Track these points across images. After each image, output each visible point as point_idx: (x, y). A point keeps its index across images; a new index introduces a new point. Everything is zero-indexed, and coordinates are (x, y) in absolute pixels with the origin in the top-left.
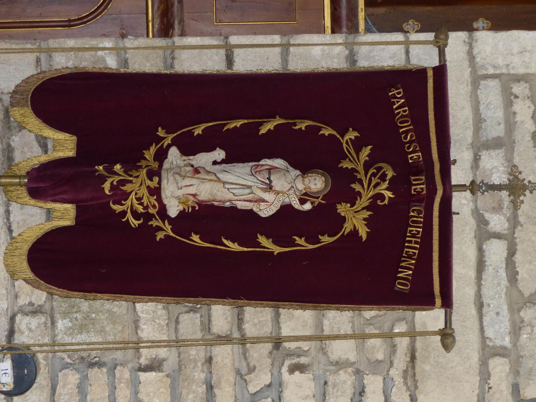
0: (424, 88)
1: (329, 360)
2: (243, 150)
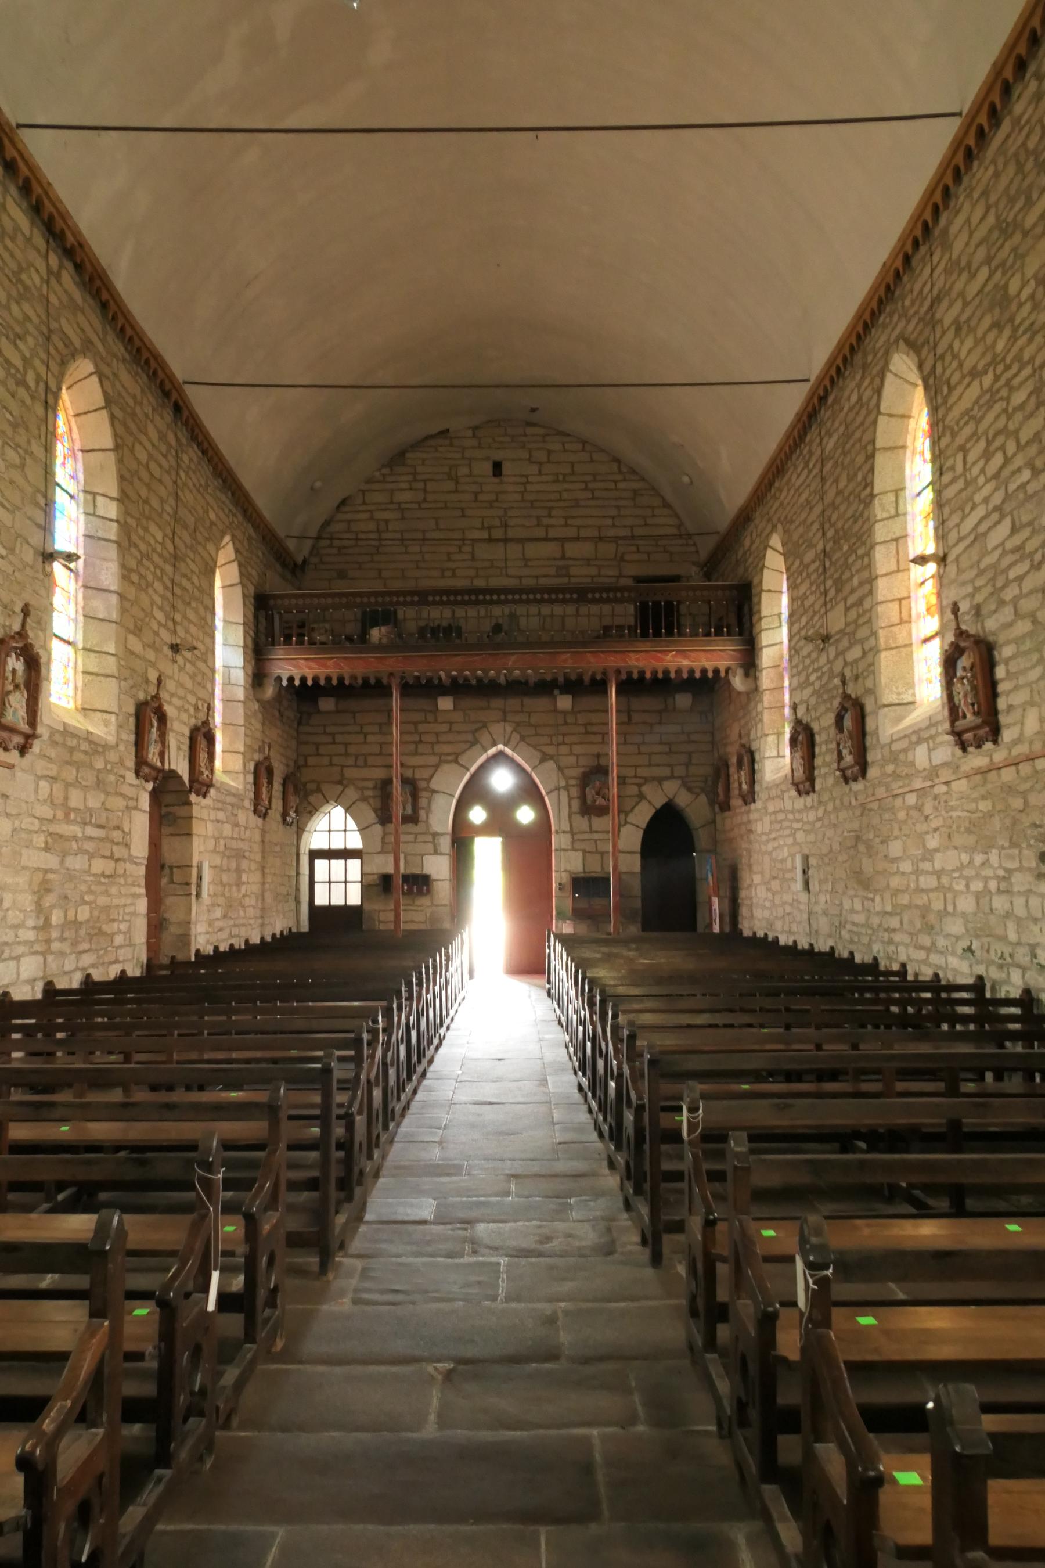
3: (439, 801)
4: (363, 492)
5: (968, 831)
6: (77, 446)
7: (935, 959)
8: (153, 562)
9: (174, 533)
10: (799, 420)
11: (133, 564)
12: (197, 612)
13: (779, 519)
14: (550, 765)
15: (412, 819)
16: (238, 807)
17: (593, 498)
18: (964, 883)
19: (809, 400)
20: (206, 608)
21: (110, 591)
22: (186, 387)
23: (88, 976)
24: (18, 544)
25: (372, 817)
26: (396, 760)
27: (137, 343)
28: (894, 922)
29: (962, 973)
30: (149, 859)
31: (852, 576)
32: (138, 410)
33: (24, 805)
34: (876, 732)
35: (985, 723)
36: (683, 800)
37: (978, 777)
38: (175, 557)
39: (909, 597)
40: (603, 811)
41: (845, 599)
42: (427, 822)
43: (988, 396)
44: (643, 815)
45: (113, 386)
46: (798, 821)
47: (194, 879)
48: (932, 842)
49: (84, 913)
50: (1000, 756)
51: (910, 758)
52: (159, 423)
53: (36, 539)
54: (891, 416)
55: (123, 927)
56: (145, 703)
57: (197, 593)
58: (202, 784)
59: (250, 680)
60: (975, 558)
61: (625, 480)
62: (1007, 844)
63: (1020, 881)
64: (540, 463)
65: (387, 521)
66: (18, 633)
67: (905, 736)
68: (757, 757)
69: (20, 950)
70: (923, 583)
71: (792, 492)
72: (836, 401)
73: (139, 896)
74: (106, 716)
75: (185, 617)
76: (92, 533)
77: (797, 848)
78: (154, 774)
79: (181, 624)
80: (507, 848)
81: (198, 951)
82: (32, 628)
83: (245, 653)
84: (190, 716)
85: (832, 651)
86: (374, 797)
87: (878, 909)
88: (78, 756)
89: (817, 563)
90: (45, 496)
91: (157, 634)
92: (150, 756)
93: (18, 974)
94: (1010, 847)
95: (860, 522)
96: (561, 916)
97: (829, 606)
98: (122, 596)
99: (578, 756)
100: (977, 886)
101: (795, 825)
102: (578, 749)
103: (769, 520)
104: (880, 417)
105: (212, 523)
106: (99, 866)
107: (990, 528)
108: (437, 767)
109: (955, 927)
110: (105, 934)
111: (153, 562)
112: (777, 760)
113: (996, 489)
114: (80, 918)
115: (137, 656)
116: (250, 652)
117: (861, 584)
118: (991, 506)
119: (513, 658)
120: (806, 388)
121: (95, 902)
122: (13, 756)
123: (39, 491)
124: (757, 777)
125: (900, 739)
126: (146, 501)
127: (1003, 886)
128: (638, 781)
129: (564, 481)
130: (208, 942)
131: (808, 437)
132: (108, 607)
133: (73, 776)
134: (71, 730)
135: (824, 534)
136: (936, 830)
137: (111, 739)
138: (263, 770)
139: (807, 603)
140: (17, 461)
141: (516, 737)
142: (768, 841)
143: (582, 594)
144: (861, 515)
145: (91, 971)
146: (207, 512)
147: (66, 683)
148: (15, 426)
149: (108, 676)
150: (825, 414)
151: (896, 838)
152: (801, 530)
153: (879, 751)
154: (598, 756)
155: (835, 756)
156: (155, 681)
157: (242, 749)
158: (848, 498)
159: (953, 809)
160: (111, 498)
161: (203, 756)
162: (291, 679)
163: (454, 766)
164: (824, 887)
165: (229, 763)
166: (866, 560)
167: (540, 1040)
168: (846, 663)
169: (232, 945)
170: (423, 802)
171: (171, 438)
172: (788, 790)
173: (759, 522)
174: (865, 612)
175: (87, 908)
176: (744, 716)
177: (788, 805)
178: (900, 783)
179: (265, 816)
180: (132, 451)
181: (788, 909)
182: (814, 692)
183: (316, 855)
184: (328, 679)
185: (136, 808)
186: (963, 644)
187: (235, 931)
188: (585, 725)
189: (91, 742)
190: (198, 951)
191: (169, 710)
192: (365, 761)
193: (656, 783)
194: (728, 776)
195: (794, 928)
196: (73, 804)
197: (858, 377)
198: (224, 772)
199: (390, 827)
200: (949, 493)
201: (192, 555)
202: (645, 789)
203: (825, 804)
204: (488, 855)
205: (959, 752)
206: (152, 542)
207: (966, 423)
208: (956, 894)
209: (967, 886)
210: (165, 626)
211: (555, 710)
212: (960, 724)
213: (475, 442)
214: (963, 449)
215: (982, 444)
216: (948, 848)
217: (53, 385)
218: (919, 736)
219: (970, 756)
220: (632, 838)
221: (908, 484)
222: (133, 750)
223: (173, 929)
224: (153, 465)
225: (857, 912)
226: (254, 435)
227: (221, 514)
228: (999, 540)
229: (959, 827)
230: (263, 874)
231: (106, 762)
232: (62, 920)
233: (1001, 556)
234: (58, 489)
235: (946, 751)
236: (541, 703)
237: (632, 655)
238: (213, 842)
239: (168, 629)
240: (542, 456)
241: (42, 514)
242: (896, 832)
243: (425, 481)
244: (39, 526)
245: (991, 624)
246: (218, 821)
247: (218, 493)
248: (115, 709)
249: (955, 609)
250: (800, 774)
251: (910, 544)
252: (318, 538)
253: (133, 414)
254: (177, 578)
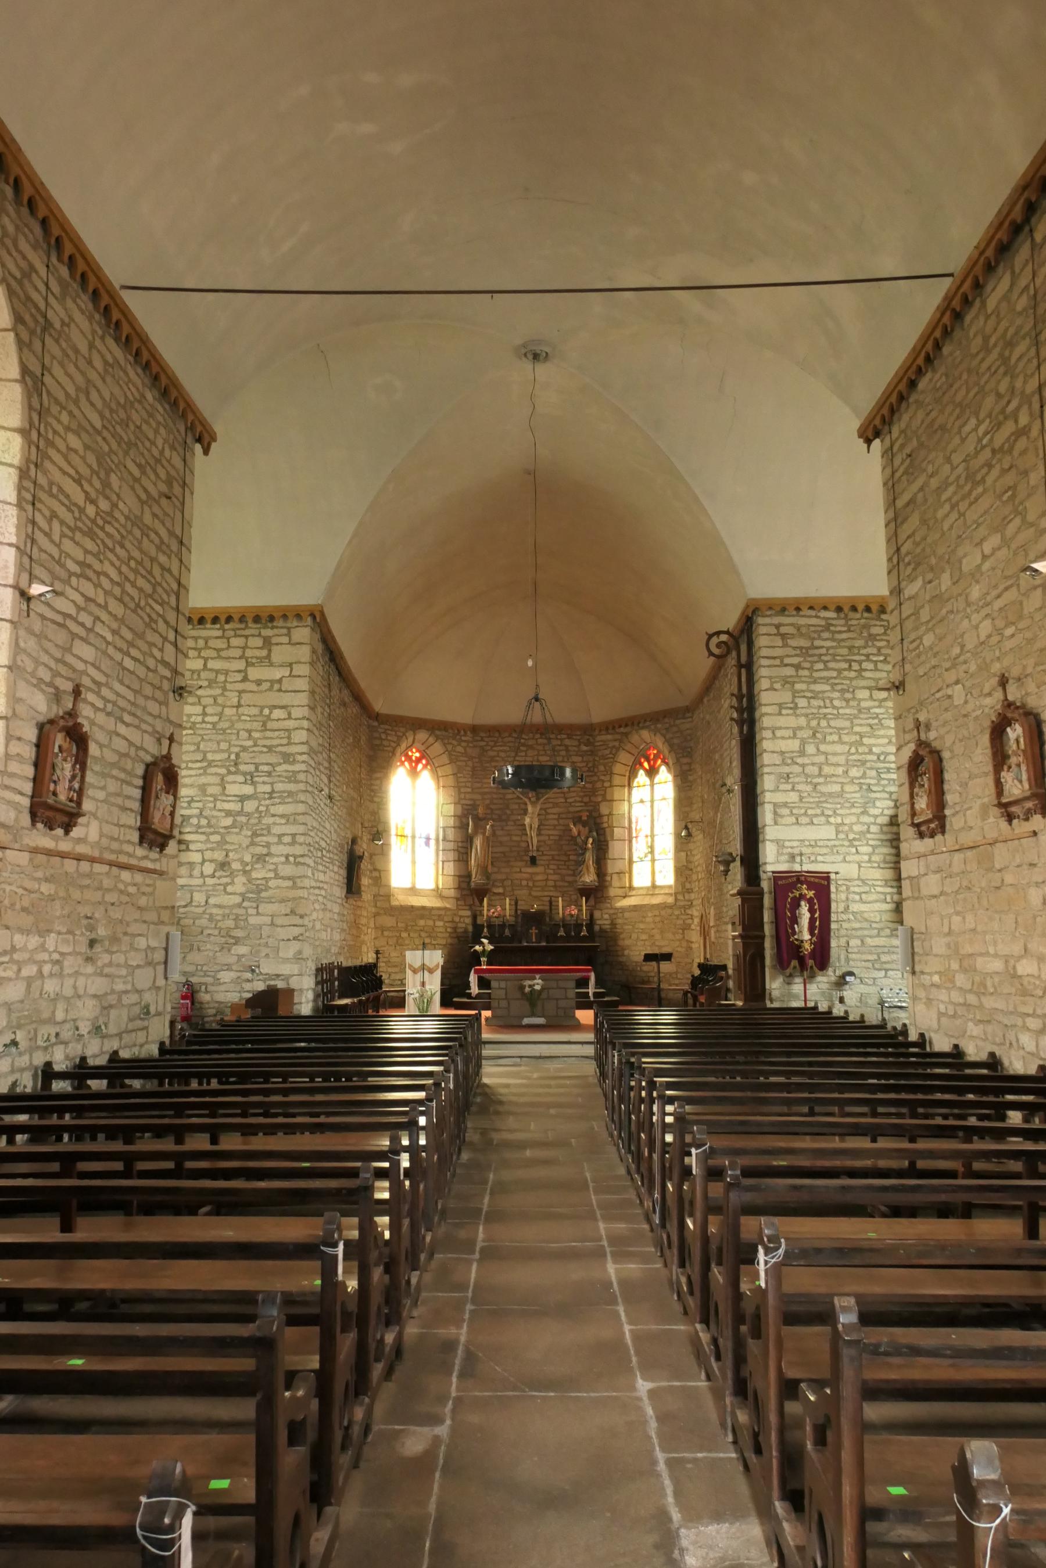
0: (778, 878)
1: (1006, 699)
2: (795, 920)
18: (15, 968)
27: (155, 369)
50: (65, 846)
63: (70, 964)
120: (947, 283)
186: (1009, 715)
229: (13, 905)
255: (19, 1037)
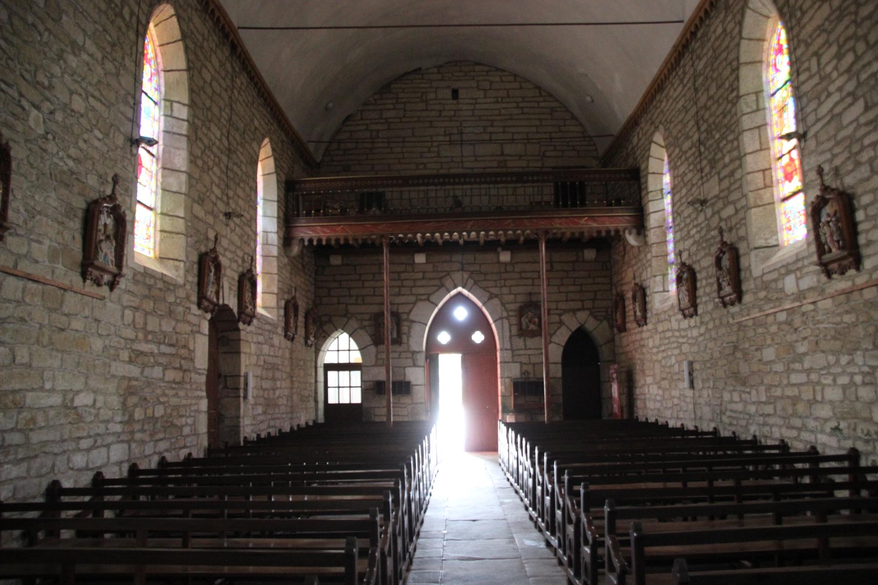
3: (416, 328)
4: (362, 111)
5: (834, 338)
6: (161, 67)
7: (806, 436)
8: (213, 153)
9: (228, 133)
10: (675, 51)
11: (199, 153)
12: (244, 190)
13: (660, 122)
14: (496, 301)
15: (398, 341)
16: (273, 333)
17: (522, 113)
18: (831, 378)
19: (683, 35)
20: (251, 188)
21: (181, 172)
22: (240, 31)
23: (163, 458)
24: (112, 131)
25: (368, 340)
26: (387, 299)
28: (769, 409)
29: (831, 447)
30: (209, 370)
31: (724, 156)
32: (205, 44)
33: (113, 328)
34: (749, 268)
35: (850, 255)
36: (591, 325)
37: (843, 297)
38: (229, 150)
39: (770, 168)
40: (536, 334)
41: (719, 173)
42: (408, 343)
43: (837, 13)
44: (562, 336)
45: (188, 27)
46: (683, 337)
47: (242, 386)
48: (802, 348)
49: (159, 411)
50: (861, 280)
51: (780, 286)
52: (218, 57)
53: (126, 127)
54: (750, 39)
55: (190, 421)
56: (206, 254)
57: (244, 177)
58: (248, 315)
59: (281, 241)
60: (832, 133)
61: (544, 101)
62: (871, 347)
64: (485, 90)
65: (378, 131)
66: (109, 196)
67: (775, 270)
68: (648, 292)
69: (110, 439)
70: (780, 158)
71: (671, 101)
72: (705, 34)
73: (201, 398)
74: (177, 263)
75: (235, 193)
76: (170, 129)
77: (683, 357)
78: (211, 307)
79: (232, 198)
80: (464, 360)
81: (245, 438)
82: (121, 194)
83: (278, 222)
84: (239, 266)
85: (709, 212)
86: (370, 326)
87: (753, 400)
88: (156, 292)
89: (694, 150)
90: (134, 98)
91: (215, 204)
92: (209, 293)
93: (108, 458)
94: (873, 349)
95: (728, 117)
96: (505, 410)
97: (705, 179)
98: (190, 176)
99: (515, 295)
100: (844, 380)
101: (681, 340)
102: (515, 290)
103: (653, 123)
104: (743, 41)
105: (256, 129)
106: (171, 375)
107: (845, 109)
108: (415, 303)
109: (825, 412)
110: (176, 426)
111: (213, 153)
112: (666, 292)
113: (849, 80)
114: (157, 415)
115: (200, 220)
116: (282, 222)
117: (732, 161)
118: (844, 93)
119: (471, 223)
120: (681, 27)
121: (168, 402)
122: (105, 290)
123: (129, 94)
124: (649, 306)
125: (770, 272)
126: (209, 109)
127: (868, 379)
128: (558, 312)
129: (502, 102)
130: (253, 431)
131: (682, 62)
132: (179, 183)
133: (152, 308)
134: (149, 272)
135: (699, 128)
136: (805, 338)
137: (181, 281)
138: (291, 305)
139: (686, 179)
140: (114, 71)
141: (471, 282)
142: (658, 353)
143: (520, 177)
144: (730, 112)
145: (166, 455)
146: (252, 120)
147: (148, 238)
148: (113, 45)
149: (178, 233)
150: (695, 45)
151: (769, 346)
152: (679, 127)
153: (752, 282)
154: (530, 294)
155: (715, 287)
156: (213, 239)
157: (276, 291)
158: (718, 101)
159: (819, 322)
160: (184, 105)
161: (248, 295)
162: (311, 241)
163: (427, 303)
164: (707, 385)
165: (265, 301)
166: (735, 143)
167: (502, 504)
168: (721, 219)
169: (269, 433)
170: (405, 329)
171: (228, 66)
172: (675, 315)
173: (644, 125)
174: (736, 181)
175: (161, 407)
176: (636, 263)
177: (675, 325)
178: (772, 305)
179: (292, 339)
180: (200, 72)
181: (676, 401)
182: (695, 242)
183: (329, 367)
184: (337, 240)
185: (199, 332)
187: (272, 423)
188: (520, 273)
189: (165, 282)
190: (245, 438)
191: (223, 260)
192: (363, 300)
193: (571, 314)
194: (624, 307)
195: (681, 415)
196: (150, 328)
197: (722, 16)
198: (264, 308)
199: (382, 347)
200: (805, 88)
201: (241, 150)
202: (564, 318)
203: (707, 324)
204: (451, 368)
205: (823, 278)
206: (213, 137)
207: (819, 35)
208: (824, 387)
209: (834, 380)
210: (221, 199)
211: (499, 262)
212: (827, 257)
213: (440, 77)
214: (817, 55)
215: (834, 49)
216: (815, 351)
217: (143, 19)
218: (791, 267)
219: (833, 282)
220: (556, 353)
221: (765, 87)
222: (196, 288)
223: (227, 422)
224: (214, 84)
225: (736, 402)
226: (288, 65)
227: (263, 123)
228: (854, 117)
229: (825, 336)
230: (292, 382)
231: (177, 298)
232: (143, 416)
233: (856, 129)
234: (143, 95)
235: (812, 278)
236: (489, 257)
237: (556, 220)
238: (255, 357)
239: (223, 201)
240: (487, 85)
241: (131, 111)
242: (769, 342)
243: (404, 103)
244: (129, 119)
245: (849, 181)
246: (259, 343)
247: (261, 108)
248: (183, 258)
249: (820, 171)
250: (686, 302)
251: (769, 130)
252: (330, 143)
253: (202, 47)
254: (230, 165)
255: (843, 425)
